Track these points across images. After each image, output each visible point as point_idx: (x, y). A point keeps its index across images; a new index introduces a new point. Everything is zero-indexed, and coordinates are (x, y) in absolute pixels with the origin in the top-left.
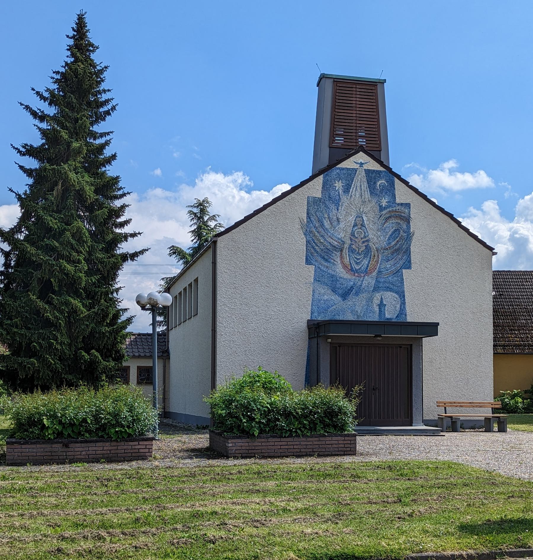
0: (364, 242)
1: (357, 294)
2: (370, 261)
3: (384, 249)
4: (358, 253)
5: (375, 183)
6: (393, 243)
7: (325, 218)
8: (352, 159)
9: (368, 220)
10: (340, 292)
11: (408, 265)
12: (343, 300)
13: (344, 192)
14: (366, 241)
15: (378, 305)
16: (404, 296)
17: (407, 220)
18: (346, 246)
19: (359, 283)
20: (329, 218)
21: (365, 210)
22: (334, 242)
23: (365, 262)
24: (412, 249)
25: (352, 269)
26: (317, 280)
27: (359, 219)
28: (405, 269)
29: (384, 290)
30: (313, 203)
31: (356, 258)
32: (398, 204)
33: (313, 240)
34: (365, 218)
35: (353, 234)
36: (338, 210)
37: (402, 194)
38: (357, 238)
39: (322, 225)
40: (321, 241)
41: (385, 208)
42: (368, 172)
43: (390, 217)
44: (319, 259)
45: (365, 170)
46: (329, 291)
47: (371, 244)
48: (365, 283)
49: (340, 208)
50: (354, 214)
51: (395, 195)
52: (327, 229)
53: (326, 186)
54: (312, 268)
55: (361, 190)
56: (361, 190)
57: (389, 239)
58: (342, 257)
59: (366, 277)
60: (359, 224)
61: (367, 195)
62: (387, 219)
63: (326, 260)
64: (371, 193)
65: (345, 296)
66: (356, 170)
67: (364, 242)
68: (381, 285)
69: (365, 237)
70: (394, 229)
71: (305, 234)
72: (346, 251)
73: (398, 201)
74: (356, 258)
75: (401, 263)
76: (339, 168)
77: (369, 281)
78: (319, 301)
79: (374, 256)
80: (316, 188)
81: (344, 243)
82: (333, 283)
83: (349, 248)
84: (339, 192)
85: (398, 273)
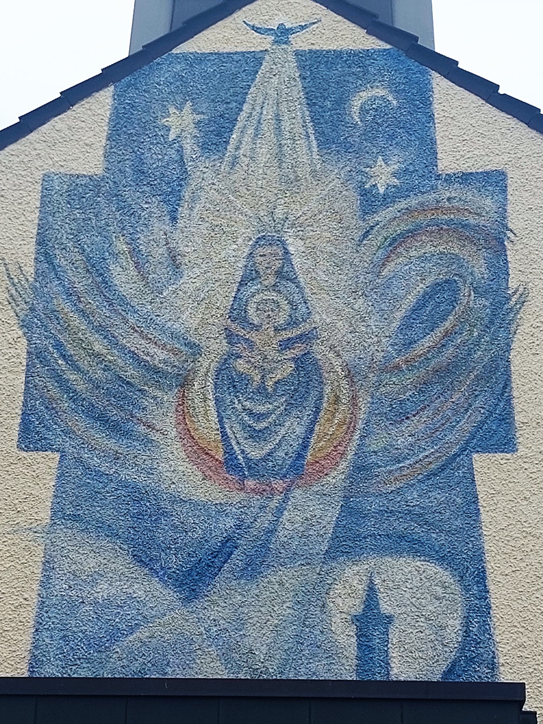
0: (286, 345)
1: (252, 570)
2: (313, 422)
3: (383, 371)
4: (261, 390)
5: (341, 102)
6: (427, 342)
7: (116, 255)
8: (240, 16)
9: (311, 251)
10: (174, 561)
11: (498, 433)
12: (187, 600)
13: (205, 147)
14: (300, 337)
15: (356, 619)
16: (481, 577)
17: (495, 242)
18: (207, 364)
19: (265, 521)
20: (135, 252)
21: (297, 210)
22: (153, 349)
23: (294, 427)
24: (520, 361)
25: (230, 463)
26: (69, 511)
27: (268, 250)
28: (485, 450)
29: (382, 551)
30: (69, 203)
31: (251, 413)
32: (449, 179)
33: (59, 346)
34: (294, 246)
35: (238, 313)
36: (174, 219)
37: (463, 134)
38: (257, 328)
39: (104, 285)
40: (97, 347)
41: (387, 200)
42: (313, 64)
43: (412, 233)
44: (80, 424)
45: (297, 53)
46: (122, 563)
47: (319, 350)
48: (291, 521)
49: (183, 211)
50: (246, 232)
51: (433, 142)
52: (122, 299)
53: (122, 130)
54: (47, 463)
55: (278, 131)
56: (278, 131)
57: (406, 325)
58: (184, 412)
59: (297, 493)
60: (270, 266)
61: (306, 153)
62: (396, 243)
63: (115, 428)
64: (325, 142)
65: (194, 579)
66: (255, 59)
67: (286, 345)
68: (369, 526)
69: (293, 323)
70: (430, 281)
71: (25, 325)
72: (203, 387)
73: (446, 163)
74: (251, 413)
75: (466, 425)
76: (185, 57)
77: (309, 512)
78: (74, 606)
79: (337, 400)
80: (81, 145)
81: (195, 350)
82: (140, 526)
83: (219, 371)
84: (180, 151)
85: (453, 473)
